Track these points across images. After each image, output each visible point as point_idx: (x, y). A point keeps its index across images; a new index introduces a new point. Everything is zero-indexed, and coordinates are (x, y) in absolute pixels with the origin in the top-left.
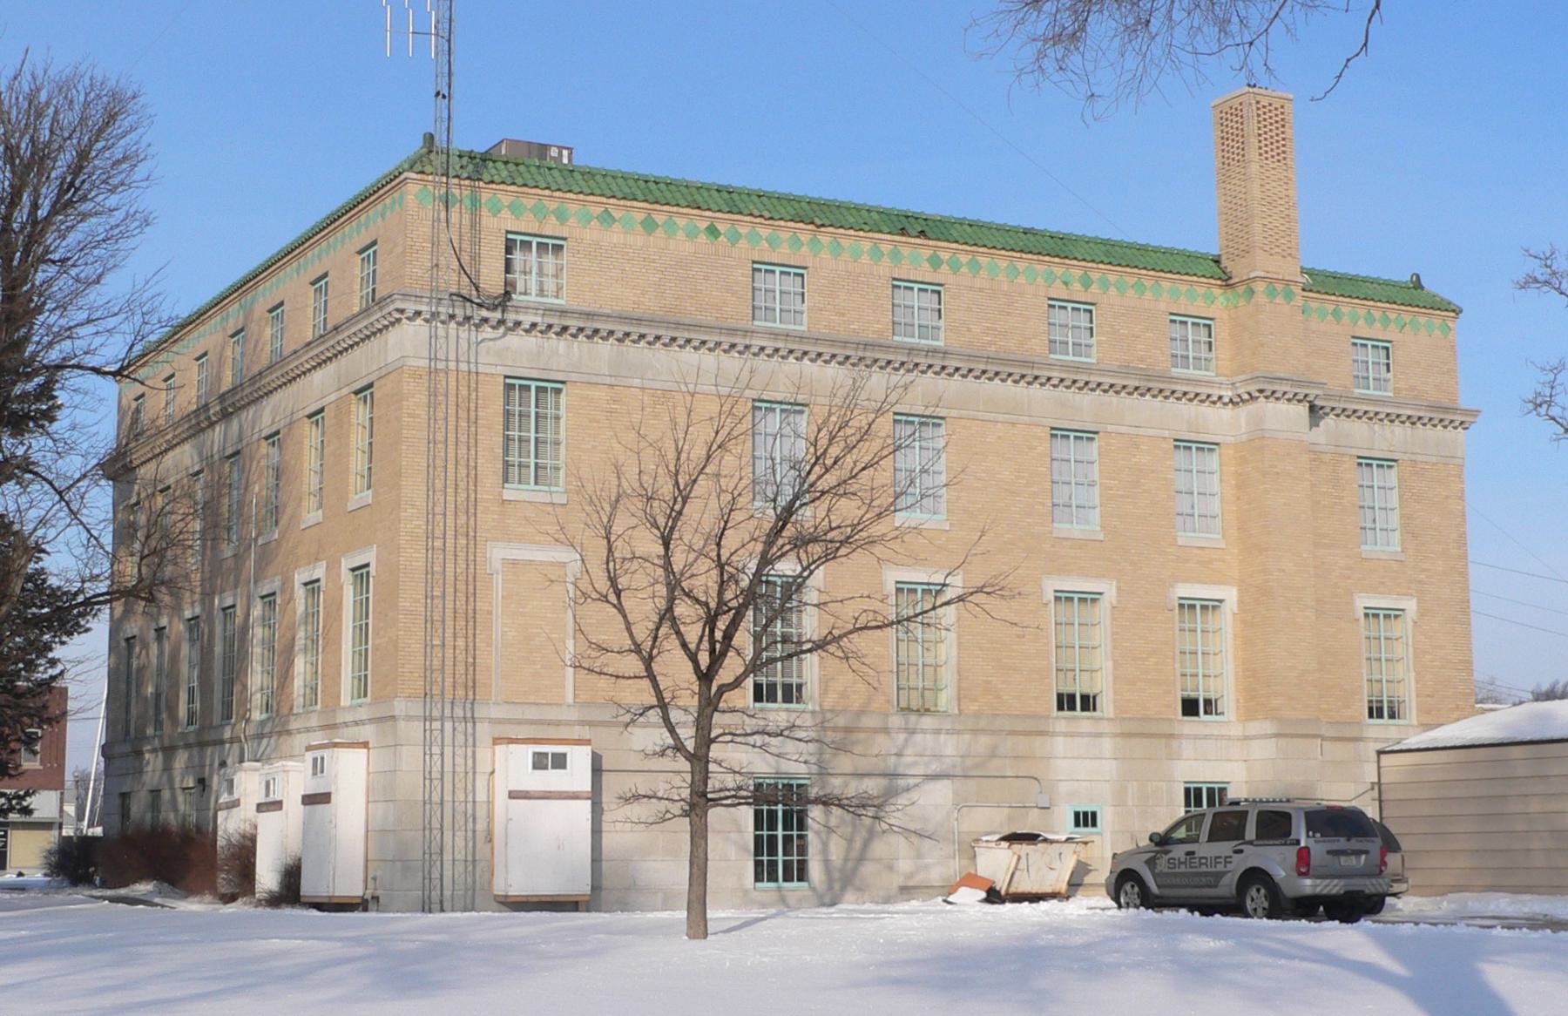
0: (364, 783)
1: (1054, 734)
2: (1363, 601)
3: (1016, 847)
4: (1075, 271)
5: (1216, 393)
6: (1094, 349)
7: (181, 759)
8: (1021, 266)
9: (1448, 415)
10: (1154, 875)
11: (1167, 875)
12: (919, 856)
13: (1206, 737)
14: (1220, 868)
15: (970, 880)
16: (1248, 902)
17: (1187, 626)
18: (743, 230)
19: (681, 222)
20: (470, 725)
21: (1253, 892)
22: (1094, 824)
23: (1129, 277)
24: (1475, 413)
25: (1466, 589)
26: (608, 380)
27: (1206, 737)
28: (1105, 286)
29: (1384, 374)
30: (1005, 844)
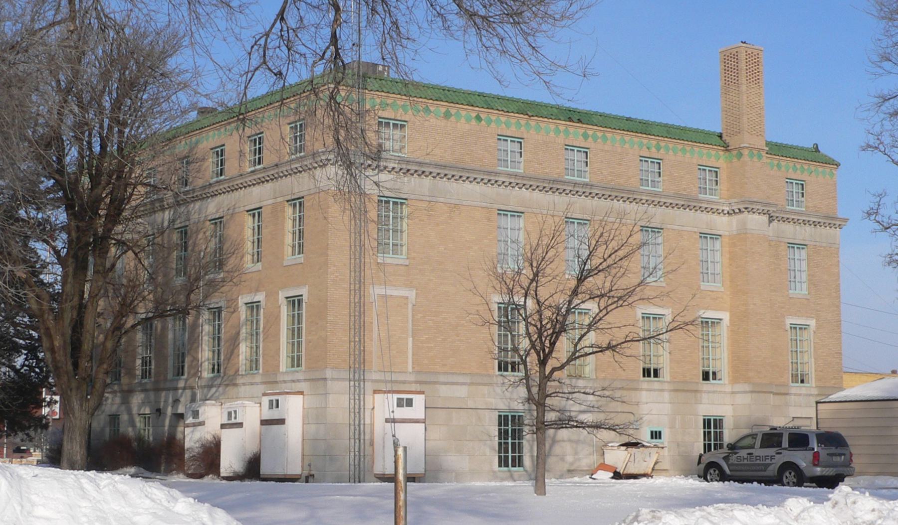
0: (301, 414)
1: (642, 389)
2: (790, 320)
3: (630, 449)
4: (653, 141)
5: (721, 208)
6: (522, 164)
7: (137, 399)
8: (627, 138)
9: (832, 221)
10: (729, 466)
11: (737, 465)
12: (576, 453)
13: (714, 392)
14: (768, 461)
15: (603, 467)
16: (784, 478)
17: (705, 332)
18: (493, 118)
19: (463, 113)
20: (362, 383)
21: (787, 474)
22: (660, 438)
23: (679, 145)
24: (846, 220)
25: (839, 315)
26: (428, 199)
27: (714, 392)
28: (667, 149)
29: (583, 168)
30: (624, 448)
